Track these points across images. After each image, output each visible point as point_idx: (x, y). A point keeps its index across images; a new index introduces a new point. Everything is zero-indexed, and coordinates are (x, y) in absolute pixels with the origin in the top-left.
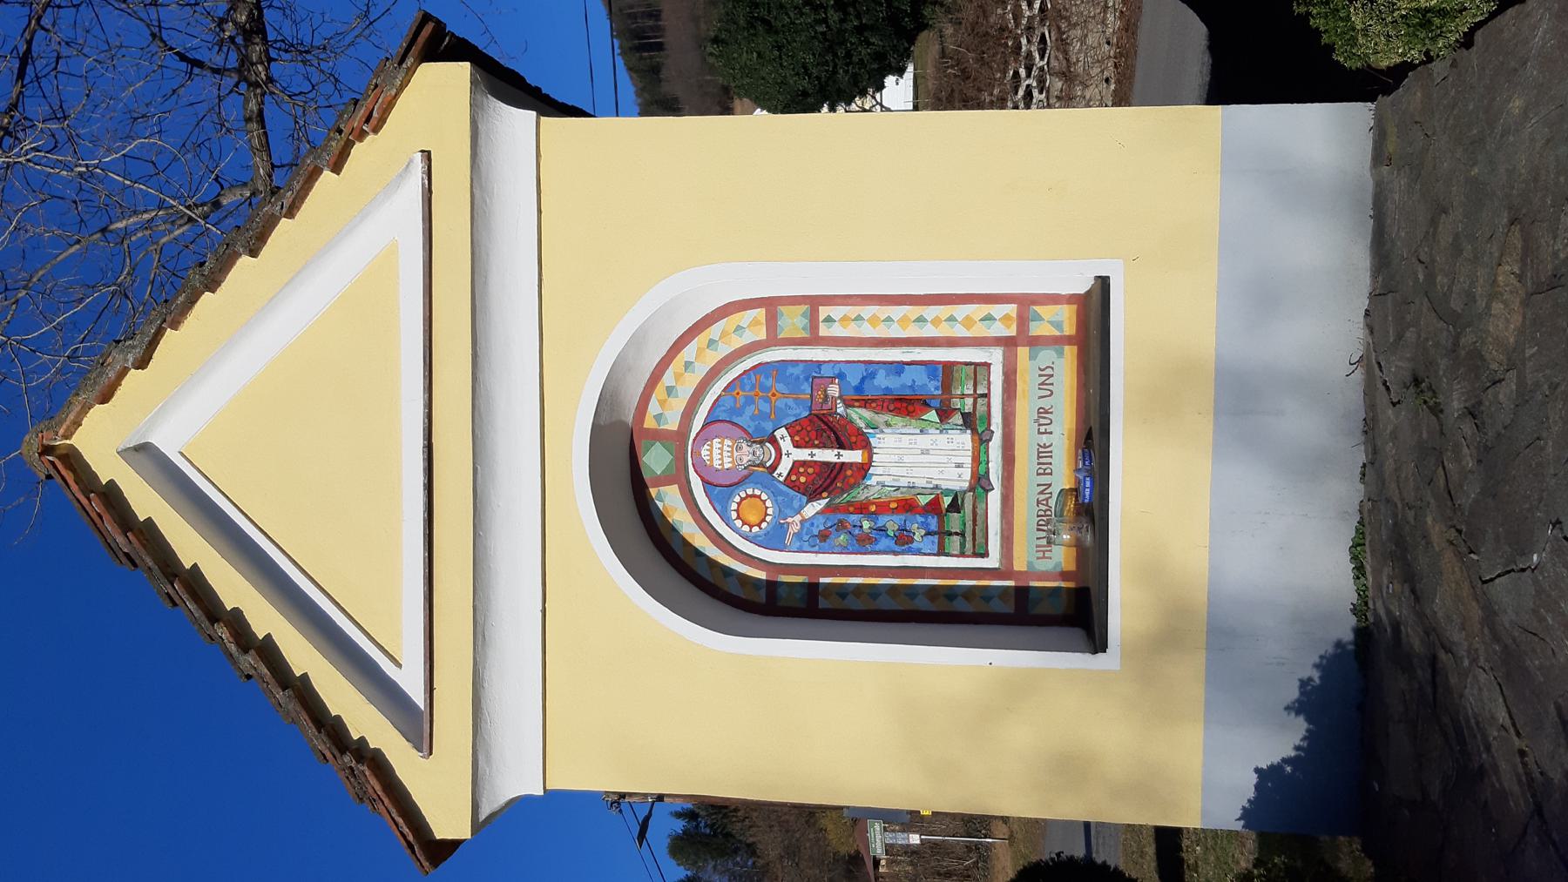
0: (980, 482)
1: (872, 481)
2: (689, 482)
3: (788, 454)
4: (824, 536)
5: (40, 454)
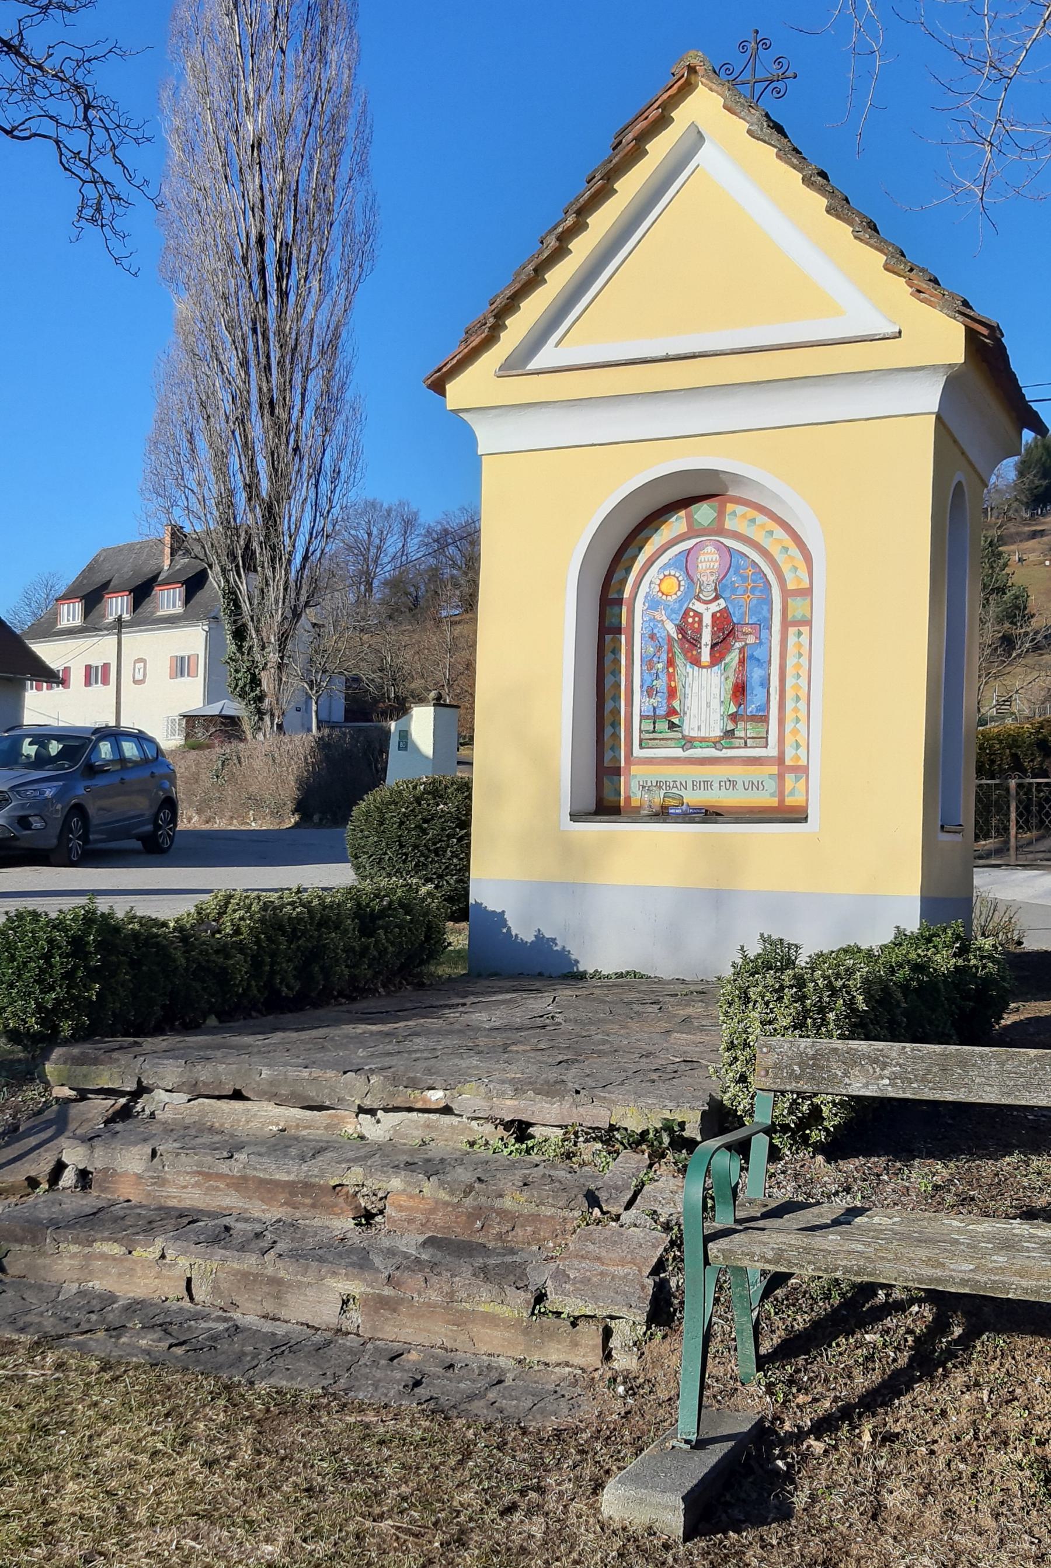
0: (688, 742)
1: (689, 669)
2: (689, 538)
3: (707, 609)
4: (652, 637)
5: (689, 66)
